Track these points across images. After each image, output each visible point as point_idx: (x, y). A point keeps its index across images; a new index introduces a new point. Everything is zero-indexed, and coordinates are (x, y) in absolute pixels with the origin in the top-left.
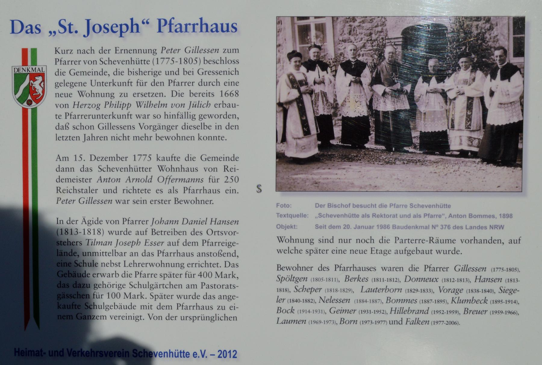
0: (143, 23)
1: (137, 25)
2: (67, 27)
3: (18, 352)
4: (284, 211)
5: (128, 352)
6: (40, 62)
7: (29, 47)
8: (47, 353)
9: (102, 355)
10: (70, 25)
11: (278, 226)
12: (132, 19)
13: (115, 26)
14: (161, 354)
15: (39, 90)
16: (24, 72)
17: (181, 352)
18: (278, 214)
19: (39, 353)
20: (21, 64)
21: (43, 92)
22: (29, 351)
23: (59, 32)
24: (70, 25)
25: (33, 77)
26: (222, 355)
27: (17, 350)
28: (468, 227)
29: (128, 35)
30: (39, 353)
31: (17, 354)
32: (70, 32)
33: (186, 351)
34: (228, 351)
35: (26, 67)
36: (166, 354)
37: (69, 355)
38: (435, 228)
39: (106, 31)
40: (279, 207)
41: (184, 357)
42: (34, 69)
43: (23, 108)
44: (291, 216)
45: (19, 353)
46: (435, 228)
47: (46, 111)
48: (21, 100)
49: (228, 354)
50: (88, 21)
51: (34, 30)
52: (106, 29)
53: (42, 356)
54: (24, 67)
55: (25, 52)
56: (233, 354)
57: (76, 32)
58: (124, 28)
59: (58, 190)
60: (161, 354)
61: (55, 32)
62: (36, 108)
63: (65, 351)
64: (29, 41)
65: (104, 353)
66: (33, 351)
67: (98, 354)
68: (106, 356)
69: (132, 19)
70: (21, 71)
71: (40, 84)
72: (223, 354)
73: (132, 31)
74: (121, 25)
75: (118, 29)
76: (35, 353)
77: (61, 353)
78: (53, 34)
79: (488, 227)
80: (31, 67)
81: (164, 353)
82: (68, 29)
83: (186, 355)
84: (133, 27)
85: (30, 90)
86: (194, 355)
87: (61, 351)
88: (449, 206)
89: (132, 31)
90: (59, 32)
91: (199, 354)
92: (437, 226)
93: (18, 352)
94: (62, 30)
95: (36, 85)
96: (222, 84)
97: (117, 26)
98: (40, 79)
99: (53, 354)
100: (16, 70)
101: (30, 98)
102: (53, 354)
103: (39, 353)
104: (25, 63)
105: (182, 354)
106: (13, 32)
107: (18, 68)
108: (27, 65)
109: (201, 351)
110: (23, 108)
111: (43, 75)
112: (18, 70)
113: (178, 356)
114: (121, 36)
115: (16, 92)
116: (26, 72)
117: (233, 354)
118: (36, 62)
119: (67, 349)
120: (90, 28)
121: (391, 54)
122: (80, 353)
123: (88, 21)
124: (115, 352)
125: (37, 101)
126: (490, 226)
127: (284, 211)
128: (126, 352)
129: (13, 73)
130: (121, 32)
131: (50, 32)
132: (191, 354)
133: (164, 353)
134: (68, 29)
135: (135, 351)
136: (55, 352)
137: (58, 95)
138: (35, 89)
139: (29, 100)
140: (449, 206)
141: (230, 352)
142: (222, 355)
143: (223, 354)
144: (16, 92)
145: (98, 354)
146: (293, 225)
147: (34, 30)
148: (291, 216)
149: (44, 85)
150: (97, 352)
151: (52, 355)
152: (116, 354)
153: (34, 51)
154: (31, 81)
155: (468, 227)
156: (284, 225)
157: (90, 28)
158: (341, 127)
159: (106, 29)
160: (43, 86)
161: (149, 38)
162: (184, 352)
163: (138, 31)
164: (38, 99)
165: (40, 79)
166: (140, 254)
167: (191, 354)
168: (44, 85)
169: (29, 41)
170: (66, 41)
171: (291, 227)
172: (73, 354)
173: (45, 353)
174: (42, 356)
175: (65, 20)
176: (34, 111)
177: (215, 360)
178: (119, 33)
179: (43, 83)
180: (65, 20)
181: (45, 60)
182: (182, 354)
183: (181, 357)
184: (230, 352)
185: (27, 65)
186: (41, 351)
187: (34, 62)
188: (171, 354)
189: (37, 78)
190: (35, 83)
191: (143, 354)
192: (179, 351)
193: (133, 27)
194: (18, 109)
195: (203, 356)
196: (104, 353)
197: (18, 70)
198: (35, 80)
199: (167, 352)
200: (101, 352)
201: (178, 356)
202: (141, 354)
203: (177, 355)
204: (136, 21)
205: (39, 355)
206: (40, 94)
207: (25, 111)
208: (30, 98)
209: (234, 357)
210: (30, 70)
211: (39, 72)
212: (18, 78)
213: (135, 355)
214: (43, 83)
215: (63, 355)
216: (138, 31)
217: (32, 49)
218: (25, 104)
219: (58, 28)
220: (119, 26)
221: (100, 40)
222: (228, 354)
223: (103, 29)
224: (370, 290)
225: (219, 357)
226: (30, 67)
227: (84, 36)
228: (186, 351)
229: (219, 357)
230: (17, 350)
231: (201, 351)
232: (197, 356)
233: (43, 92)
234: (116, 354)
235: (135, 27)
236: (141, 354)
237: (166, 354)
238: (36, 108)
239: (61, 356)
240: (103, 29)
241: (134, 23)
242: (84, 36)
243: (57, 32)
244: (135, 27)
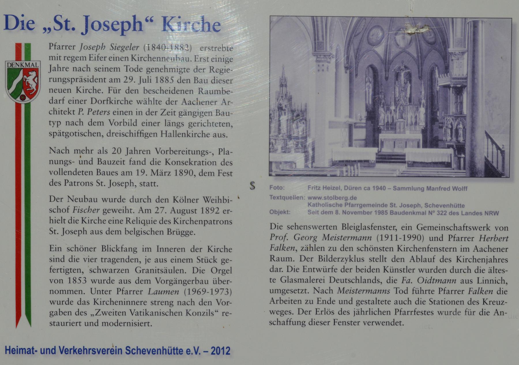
0: (147, 20)
1: (140, 23)
2: (64, 24)
3: (9, 350)
4: (277, 193)
5: (121, 349)
6: (34, 56)
7: (23, 42)
8: (39, 351)
9: (94, 353)
10: (66, 21)
11: (272, 212)
12: (134, 17)
13: (116, 23)
14: (283, 73)
15: (33, 85)
16: (17, 67)
17: (174, 349)
18: (271, 196)
19: (31, 351)
20: (14, 58)
21: (37, 87)
22: (20, 349)
23: (55, 29)
24: (66, 21)
25: (27, 72)
26: (215, 352)
27: (8, 348)
28: (464, 213)
29: (130, 34)
30: (31, 351)
31: (8, 352)
32: (67, 29)
33: (179, 348)
34: (221, 348)
35: (20, 62)
36: (159, 351)
37: (62, 353)
38: (431, 214)
39: (106, 28)
40: (272, 189)
41: (177, 354)
42: (27, 64)
43: (16, 103)
44: (284, 198)
45: (10, 351)
46: (431, 214)
47: (39, 106)
48: (14, 95)
49: (222, 351)
50: (87, 17)
51: (28, 26)
53: (33, 353)
54: (17, 62)
55: (18, 46)
56: (226, 351)
57: (73, 29)
58: (126, 26)
60: (283, 73)
61: (49, 29)
62: (30, 103)
63: (57, 349)
64: (22, 37)
65: (96, 350)
66: (25, 349)
67: (91, 351)
68: (99, 353)
69: (134, 17)
70: (15, 66)
71: (34, 80)
72: (216, 351)
73: (134, 29)
74: (123, 23)
75: (119, 27)
76: (27, 351)
77: (53, 351)
78: (48, 31)
79: (483, 213)
80: (25, 62)
81: (158, 350)
82: (64, 25)
83: (180, 352)
84: (136, 25)
85: (24, 85)
86: (187, 352)
87: (52, 349)
88: (463, 206)
89: (134, 29)
90: (55, 29)
91: (192, 351)
92: (434, 212)
93: (9, 350)
94: (58, 27)
95: (30, 80)
96: (92, 70)
97: (118, 24)
98: (34, 74)
100: (9, 65)
101: (23, 93)
103: (30, 351)
104: (18, 57)
105: (175, 351)
106: (7, 28)
107: (11, 62)
108: (21, 60)
109: (194, 347)
110: (16, 103)
111: (36, 70)
112: (12, 65)
113: (171, 353)
114: (123, 34)
115: (9, 87)
116: (20, 67)
117: (226, 351)
118: (30, 56)
119: (60, 347)
120: (89, 25)
122: (72, 351)
123: (87, 17)
124: (108, 349)
125: (31, 97)
126: (486, 212)
127: (277, 193)
128: (119, 350)
129: (7, 68)
130: (123, 30)
131: (45, 29)
132: (185, 351)
133: (158, 350)
134: (64, 25)
135: (128, 348)
136: (47, 349)
137: (52, 91)
138: (29, 84)
139: (23, 95)
140: (463, 206)
141: (223, 348)
142: (215, 352)
143: (216, 351)
144: (9, 87)
145: (91, 351)
146: (286, 210)
147: (28, 26)
148: (284, 198)
149: (38, 80)
150: (90, 349)
151: (44, 353)
152: (109, 351)
153: (28, 46)
154: (25, 76)
155: (464, 213)
156: (277, 210)
157: (89, 25)
160: (36, 81)
162: (177, 349)
163: (141, 30)
164: (31, 94)
165: (34, 74)
166: (73, 313)
167: (185, 351)
168: (38, 80)
169: (22, 37)
170: (62, 37)
171: (285, 212)
172: (65, 351)
173: (36, 351)
174: (33, 353)
175: (61, 16)
176: (28, 106)
178: (120, 31)
179: (36, 78)
180: (61, 16)
181: (40, 55)
182: (175, 351)
183: (174, 354)
184: (223, 348)
185: (21, 60)
186: (33, 349)
187: (28, 57)
188: (164, 351)
189: (30, 73)
190: (29, 78)
191: (136, 351)
192: (172, 348)
194: (10, 104)
195: (196, 353)
196: (96, 350)
197: (12, 65)
198: (28, 75)
199: (160, 349)
200: (93, 350)
201: (171, 353)
202: (134, 351)
203: (170, 352)
205: (30, 353)
206: (33, 90)
207: (18, 107)
208: (23, 93)
209: (227, 354)
210: (24, 65)
211: (32, 67)
212: (12, 73)
213: (128, 352)
214: (36, 78)
215: (55, 353)
216: (141, 30)
217: (25, 44)
218: (19, 99)
219: (53, 25)
220: (120, 24)
221: (96, 37)
222: (222, 351)
223: (103, 26)
225: (212, 354)
227: (82, 34)
228: (179, 348)
229: (212, 354)
230: (8, 348)
231: (194, 347)
232: (191, 353)
233: (37, 87)
234: (109, 351)
235: (138, 25)
236: (134, 351)
237: (159, 351)
238: (30, 103)
239: (53, 354)
240: (103, 26)
241: (136, 21)
242: (82, 34)
243: (52, 29)
244: (138, 25)
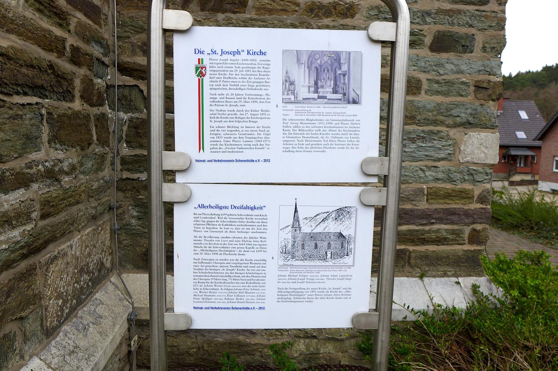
4: (285, 109)
6: (204, 63)
15: (204, 73)
19: (204, 161)
25: (202, 68)
30: (204, 161)
47: (206, 79)
48: (198, 76)
52: (228, 53)
59: (283, 130)
64: (200, 56)
72: (265, 161)
82: (215, 53)
84: (238, 53)
85: (201, 72)
99: (208, 161)
102: (208, 161)
104: (199, 63)
111: (205, 67)
120: (223, 52)
121: (290, 92)
127: (285, 109)
134: (215, 53)
143: (265, 161)
153: (202, 59)
158: (124, 276)
159: (228, 53)
161: (244, 55)
164: (204, 76)
176: (202, 79)
177: (258, 310)
181: (206, 63)
187: (202, 63)
193: (238, 53)
194: (197, 79)
204: (240, 50)
207: (199, 80)
212: (197, 69)
219: (210, 52)
224: (353, 138)
226: (201, 65)
